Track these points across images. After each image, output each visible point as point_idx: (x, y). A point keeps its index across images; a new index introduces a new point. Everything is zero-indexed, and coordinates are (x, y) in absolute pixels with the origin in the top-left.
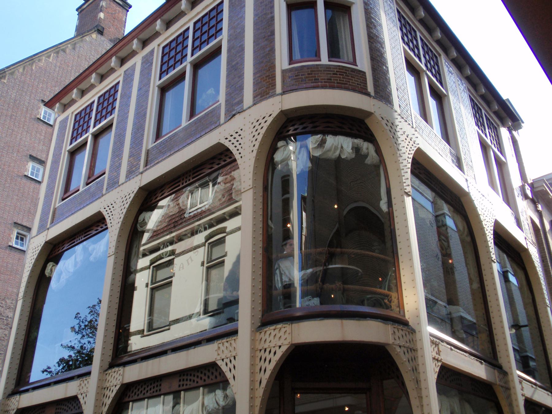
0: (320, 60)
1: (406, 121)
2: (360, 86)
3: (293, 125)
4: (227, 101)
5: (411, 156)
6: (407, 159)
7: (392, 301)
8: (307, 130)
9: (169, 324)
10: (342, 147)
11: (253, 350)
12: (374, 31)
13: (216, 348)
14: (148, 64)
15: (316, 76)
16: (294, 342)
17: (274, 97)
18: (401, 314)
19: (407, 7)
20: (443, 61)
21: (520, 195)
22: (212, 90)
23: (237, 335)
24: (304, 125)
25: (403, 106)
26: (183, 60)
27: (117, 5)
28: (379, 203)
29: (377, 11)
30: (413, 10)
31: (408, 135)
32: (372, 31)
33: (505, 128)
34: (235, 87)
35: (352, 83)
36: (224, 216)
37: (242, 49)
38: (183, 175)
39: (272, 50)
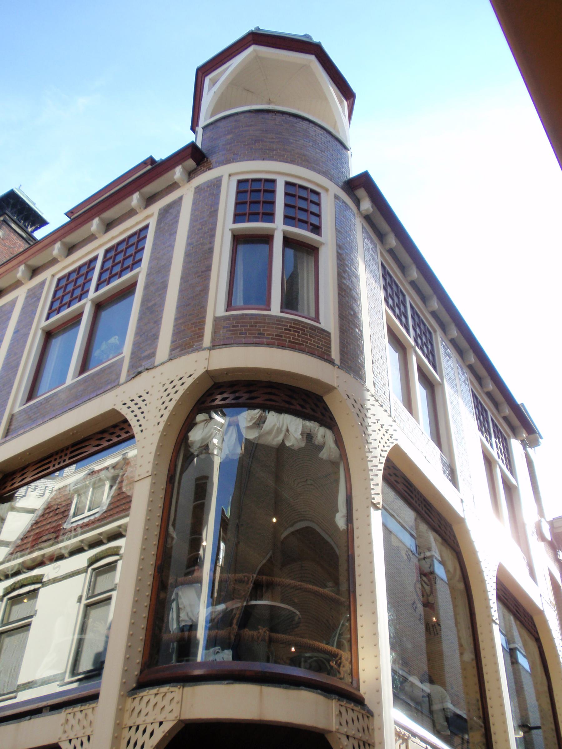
0: (270, 310)
1: (382, 406)
2: (320, 350)
3: (221, 393)
4: (133, 353)
5: (385, 454)
6: (379, 457)
7: (342, 665)
8: (241, 401)
9: (18, 689)
10: (288, 430)
11: (119, 726)
12: (348, 283)
13: (63, 721)
14: (35, 299)
15: (262, 329)
16: (184, 717)
17: (199, 351)
18: (353, 686)
19: (395, 264)
20: (439, 340)
21: (535, 534)
22: (116, 338)
23: (98, 702)
24: (237, 395)
25: (379, 385)
26: (83, 296)
27: (19, 237)
28: (334, 517)
29: (354, 258)
30: (403, 268)
31: (383, 425)
32: (345, 282)
33: (517, 441)
34: (147, 335)
35: (310, 344)
36: (119, 531)
37: (164, 287)
38: (57, 453)
39: (205, 290)
